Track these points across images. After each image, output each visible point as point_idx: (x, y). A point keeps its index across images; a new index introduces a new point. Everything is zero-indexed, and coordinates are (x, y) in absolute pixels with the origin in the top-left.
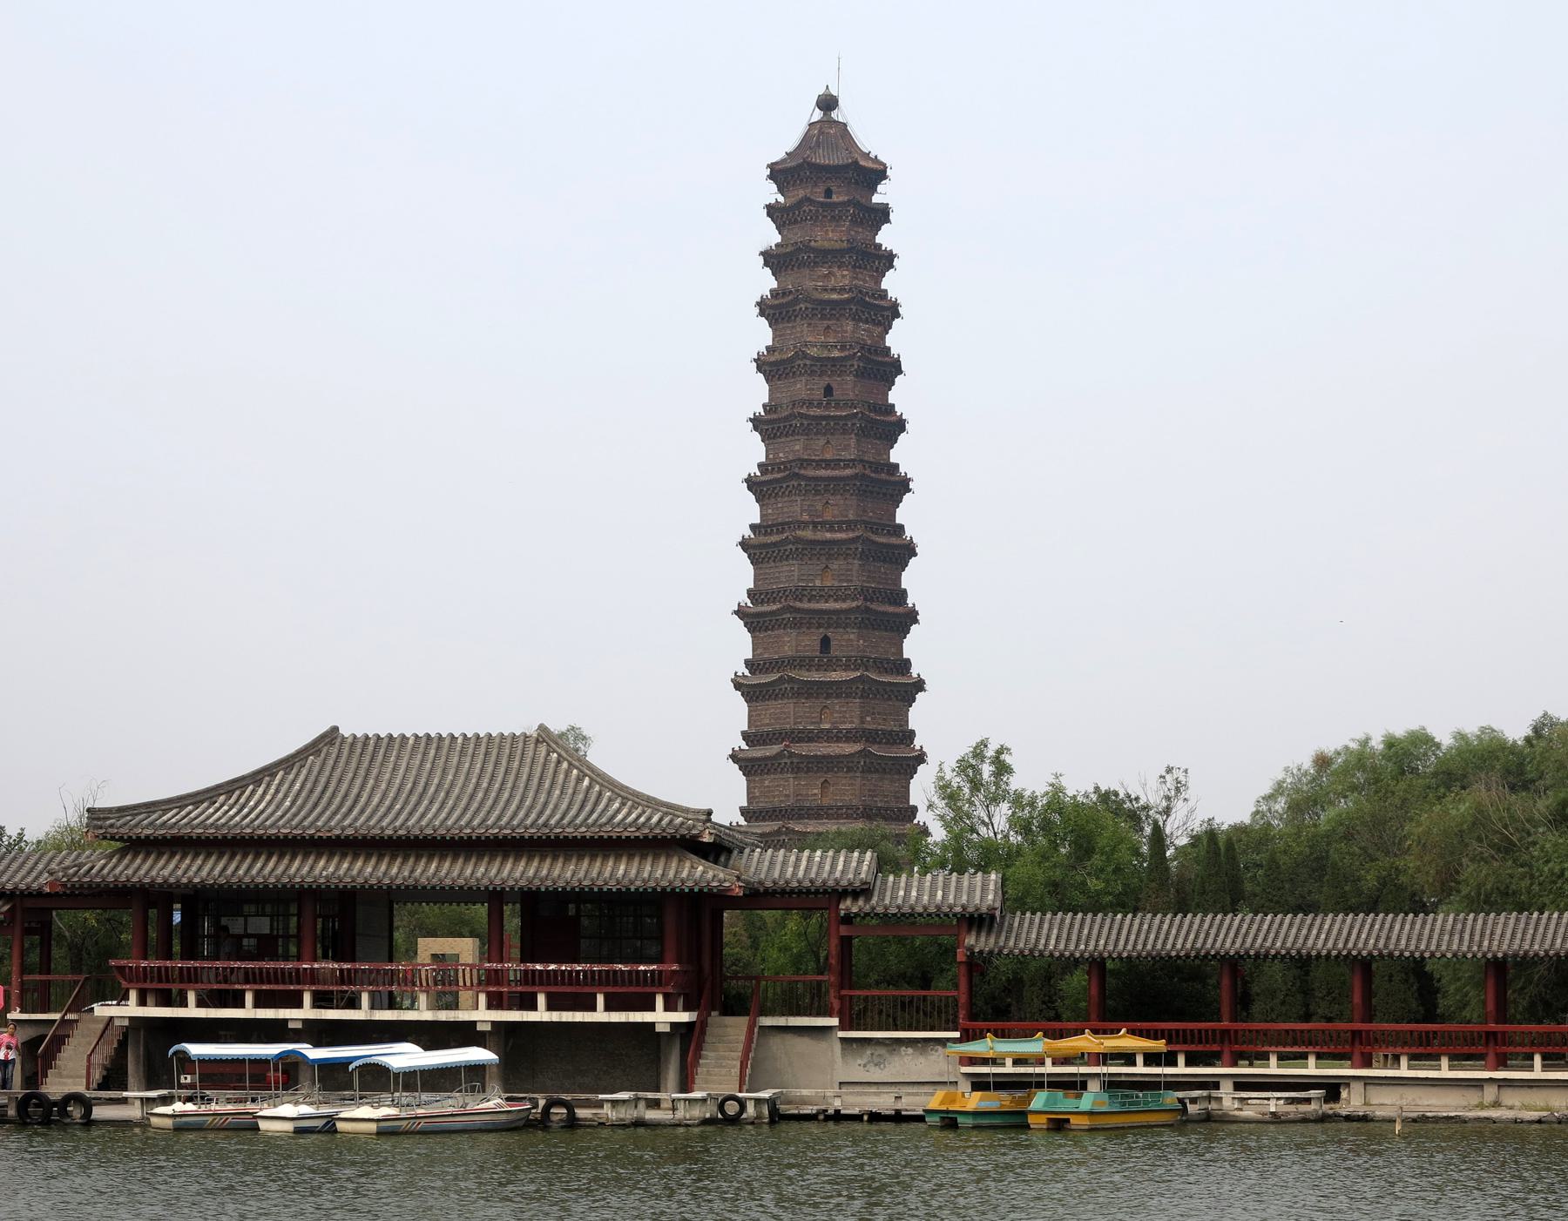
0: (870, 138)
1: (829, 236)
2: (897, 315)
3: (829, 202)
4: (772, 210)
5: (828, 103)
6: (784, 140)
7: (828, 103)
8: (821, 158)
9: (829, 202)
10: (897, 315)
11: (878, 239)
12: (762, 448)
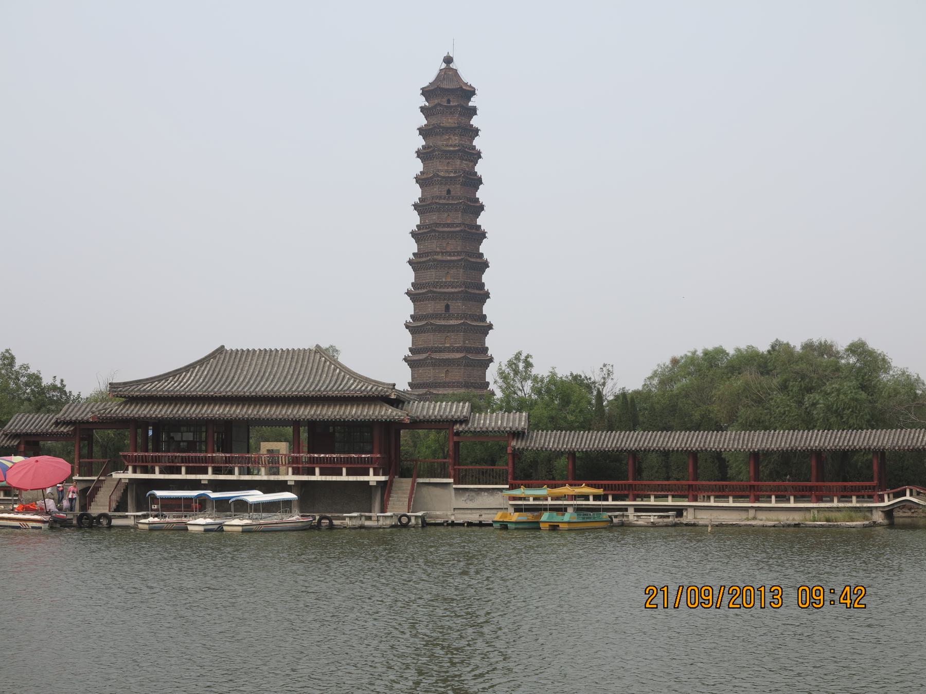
0: (468, 76)
1: (449, 121)
2: (480, 157)
3: (449, 106)
4: (423, 109)
5: (448, 60)
6: (428, 77)
7: (448, 60)
8: (446, 85)
9: (449, 106)
10: (480, 157)
11: (471, 122)
12: (412, 305)
